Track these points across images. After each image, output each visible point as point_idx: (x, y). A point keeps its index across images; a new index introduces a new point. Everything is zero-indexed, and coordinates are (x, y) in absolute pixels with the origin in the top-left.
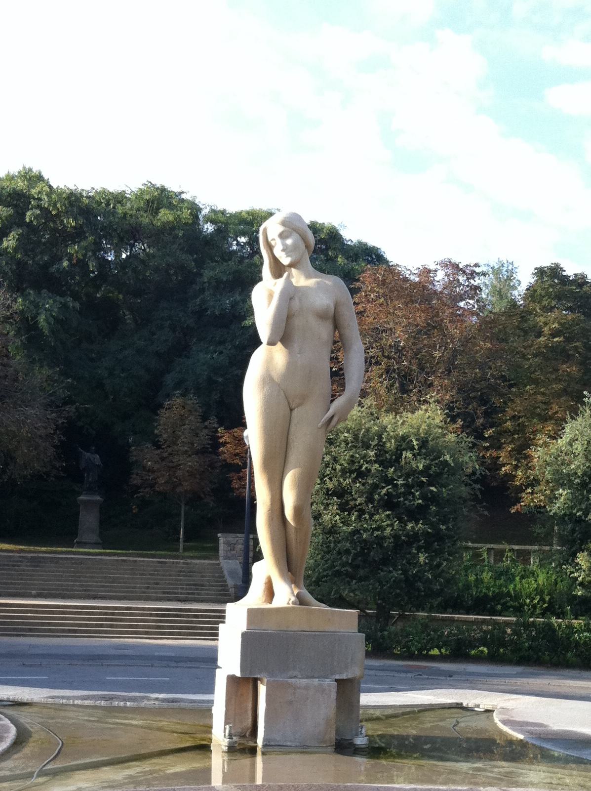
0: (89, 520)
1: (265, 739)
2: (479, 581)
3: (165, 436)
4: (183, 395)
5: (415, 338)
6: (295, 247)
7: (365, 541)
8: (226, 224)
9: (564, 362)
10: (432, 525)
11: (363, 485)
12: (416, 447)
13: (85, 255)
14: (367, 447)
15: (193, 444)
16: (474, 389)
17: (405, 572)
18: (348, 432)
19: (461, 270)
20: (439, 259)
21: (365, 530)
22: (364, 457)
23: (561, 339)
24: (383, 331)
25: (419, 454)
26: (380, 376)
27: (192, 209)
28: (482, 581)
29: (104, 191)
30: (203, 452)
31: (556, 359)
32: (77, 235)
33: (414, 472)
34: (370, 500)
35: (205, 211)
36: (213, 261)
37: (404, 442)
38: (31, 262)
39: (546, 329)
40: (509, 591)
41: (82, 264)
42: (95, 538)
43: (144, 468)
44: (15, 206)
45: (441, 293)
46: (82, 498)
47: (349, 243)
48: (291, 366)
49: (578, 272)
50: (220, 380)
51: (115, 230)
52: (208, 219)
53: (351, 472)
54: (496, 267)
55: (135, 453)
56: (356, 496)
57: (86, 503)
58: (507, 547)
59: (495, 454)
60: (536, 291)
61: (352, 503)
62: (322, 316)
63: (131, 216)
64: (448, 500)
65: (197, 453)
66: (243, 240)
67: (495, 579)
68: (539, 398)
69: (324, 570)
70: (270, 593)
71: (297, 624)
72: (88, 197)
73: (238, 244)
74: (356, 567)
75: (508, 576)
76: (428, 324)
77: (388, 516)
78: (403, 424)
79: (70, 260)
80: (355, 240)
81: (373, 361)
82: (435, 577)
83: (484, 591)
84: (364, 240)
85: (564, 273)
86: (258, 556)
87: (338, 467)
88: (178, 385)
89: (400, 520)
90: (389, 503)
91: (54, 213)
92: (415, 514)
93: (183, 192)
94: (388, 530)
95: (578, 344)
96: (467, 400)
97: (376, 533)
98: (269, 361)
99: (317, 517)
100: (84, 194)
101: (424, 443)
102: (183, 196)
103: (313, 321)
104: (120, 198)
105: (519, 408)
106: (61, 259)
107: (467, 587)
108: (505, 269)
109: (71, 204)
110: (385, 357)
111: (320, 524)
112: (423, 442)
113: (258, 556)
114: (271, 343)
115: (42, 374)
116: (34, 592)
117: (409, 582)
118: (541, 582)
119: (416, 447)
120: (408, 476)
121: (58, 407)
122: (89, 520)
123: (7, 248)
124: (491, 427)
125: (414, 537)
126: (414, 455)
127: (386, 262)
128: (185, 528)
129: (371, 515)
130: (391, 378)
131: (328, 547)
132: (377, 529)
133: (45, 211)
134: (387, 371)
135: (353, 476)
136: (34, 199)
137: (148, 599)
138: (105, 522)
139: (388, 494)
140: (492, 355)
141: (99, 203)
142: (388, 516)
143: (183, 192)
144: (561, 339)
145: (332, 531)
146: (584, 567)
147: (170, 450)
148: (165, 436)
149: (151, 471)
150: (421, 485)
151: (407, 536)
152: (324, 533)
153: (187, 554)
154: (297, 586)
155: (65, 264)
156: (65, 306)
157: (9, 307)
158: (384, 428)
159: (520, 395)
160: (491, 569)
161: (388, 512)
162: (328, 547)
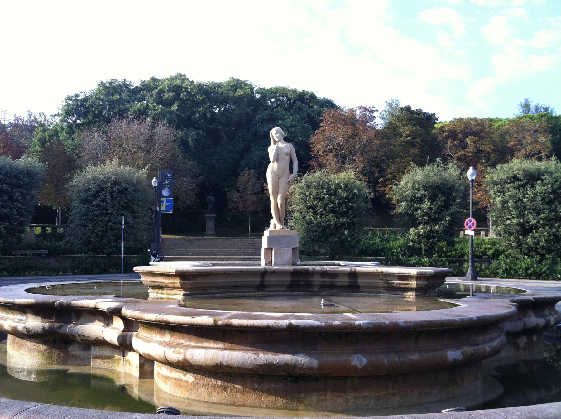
0: (210, 224)
1: (274, 263)
2: (374, 243)
3: (242, 187)
4: (249, 169)
5: (347, 140)
6: (279, 137)
7: (323, 226)
8: (265, 94)
9: (413, 148)
10: (350, 219)
11: (322, 204)
12: (343, 188)
13: (205, 111)
14: (323, 188)
15: (253, 190)
16: (373, 161)
17: (340, 238)
18: (315, 182)
19: (367, 109)
20: (359, 105)
21: (323, 222)
22: (322, 192)
23: (411, 138)
24: (334, 138)
25: (344, 190)
26: (333, 157)
27: (251, 88)
28: (376, 243)
29: (213, 83)
30: (258, 193)
31: (409, 147)
32: (203, 102)
33: (342, 198)
34: (325, 210)
35: (256, 89)
36: (260, 110)
37: (338, 186)
38: (183, 115)
39: (404, 134)
40: (387, 247)
41: (205, 115)
42: (213, 232)
43: (233, 201)
44: (176, 92)
45: (358, 120)
46: (207, 215)
47: (320, 99)
48: (279, 168)
49: (418, 108)
50: (265, 162)
51: (219, 100)
52: (257, 92)
53: (317, 199)
54: (390, 103)
55: (229, 195)
56: (319, 208)
57: (208, 217)
58: (387, 229)
59: (383, 189)
60: (399, 117)
61: (318, 211)
62: (287, 154)
63: (225, 93)
64: (357, 209)
65: (255, 194)
66: (273, 100)
67: (382, 242)
68: (402, 164)
69: (307, 239)
70: (275, 227)
71: (282, 234)
72: (206, 86)
73: (271, 102)
74: (320, 237)
75: (387, 240)
76: (353, 134)
77: (332, 216)
78: (337, 178)
79: (199, 113)
80: (322, 98)
81: (329, 151)
82: (352, 240)
83: (377, 247)
84: (326, 97)
85: (412, 109)
86: (272, 218)
87: (312, 197)
88: (247, 165)
89: (338, 217)
90: (333, 211)
91: (193, 93)
92: (343, 215)
93: (246, 81)
94: (333, 222)
95: (418, 140)
96: (371, 166)
97: (328, 223)
98: (273, 167)
99: (304, 217)
100: (205, 84)
101: (346, 186)
102: (247, 82)
103: (284, 156)
104: (219, 85)
105: (393, 169)
106: (196, 113)
107: (370, 245)
108: (394, 103)
109: (200, 89)
110: (334, 149)
111: (305, 220)
112: (346, 185)
113: (272, 218)
114: (273, 162)
115: (190, 164)
116: (191, 254)
117: (342, 242)
118: (401, 243)
119: (343, 188)
120: (340, 199)
121: (197, 177)
122: (210, 224)
123: (174, 110)
124: (382, 177)
125: (343, 224)
126: (342, 191)
127: (336, 106)
128: (251, 227)
129: (326, 216)
130: (337, 158)
131: (309, 229)
132: (328, 221)
133: (189, 93)
134: (336, 155)
135: (318, 200)
136: (184, 88)
137: (237, 255)
138: (217, 226)
139: (332, 207)
140: (382, 145)
141: (211, 88)
142: (332, 216)
143: (246, 81)
144: (411, 138)
145: (310, 223)
146: (412, 234)
147: (244, 193)
148: (242, 187)
149: (236, 202)
150: (345, 203)
151: (340, 223)
152: (307, 224)
153: (252, 237)
154: (282, 225)
155: (197, 115)
156: (199, 134)
157: (176, 136)
158: (330, 181)
159: (393, 163)
160: (380, 238)
161: (332, 214)
162: (309, 229)
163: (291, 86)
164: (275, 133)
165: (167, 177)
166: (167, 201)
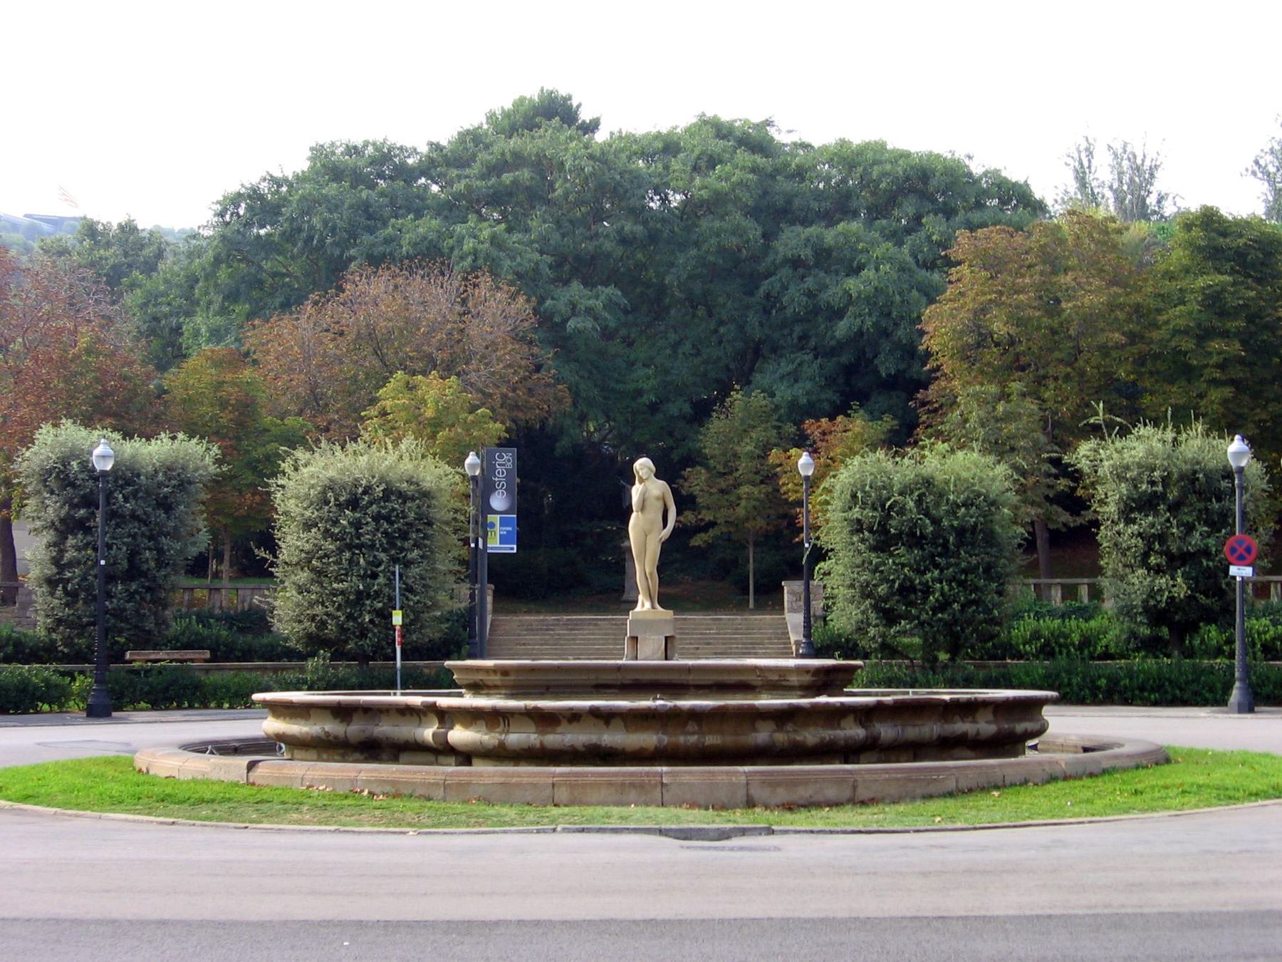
62: (658, 499)
71: (650, 617)
163: (897, 142)
164: (643, 465)
165: (500, 461)
166: (503, 523)
